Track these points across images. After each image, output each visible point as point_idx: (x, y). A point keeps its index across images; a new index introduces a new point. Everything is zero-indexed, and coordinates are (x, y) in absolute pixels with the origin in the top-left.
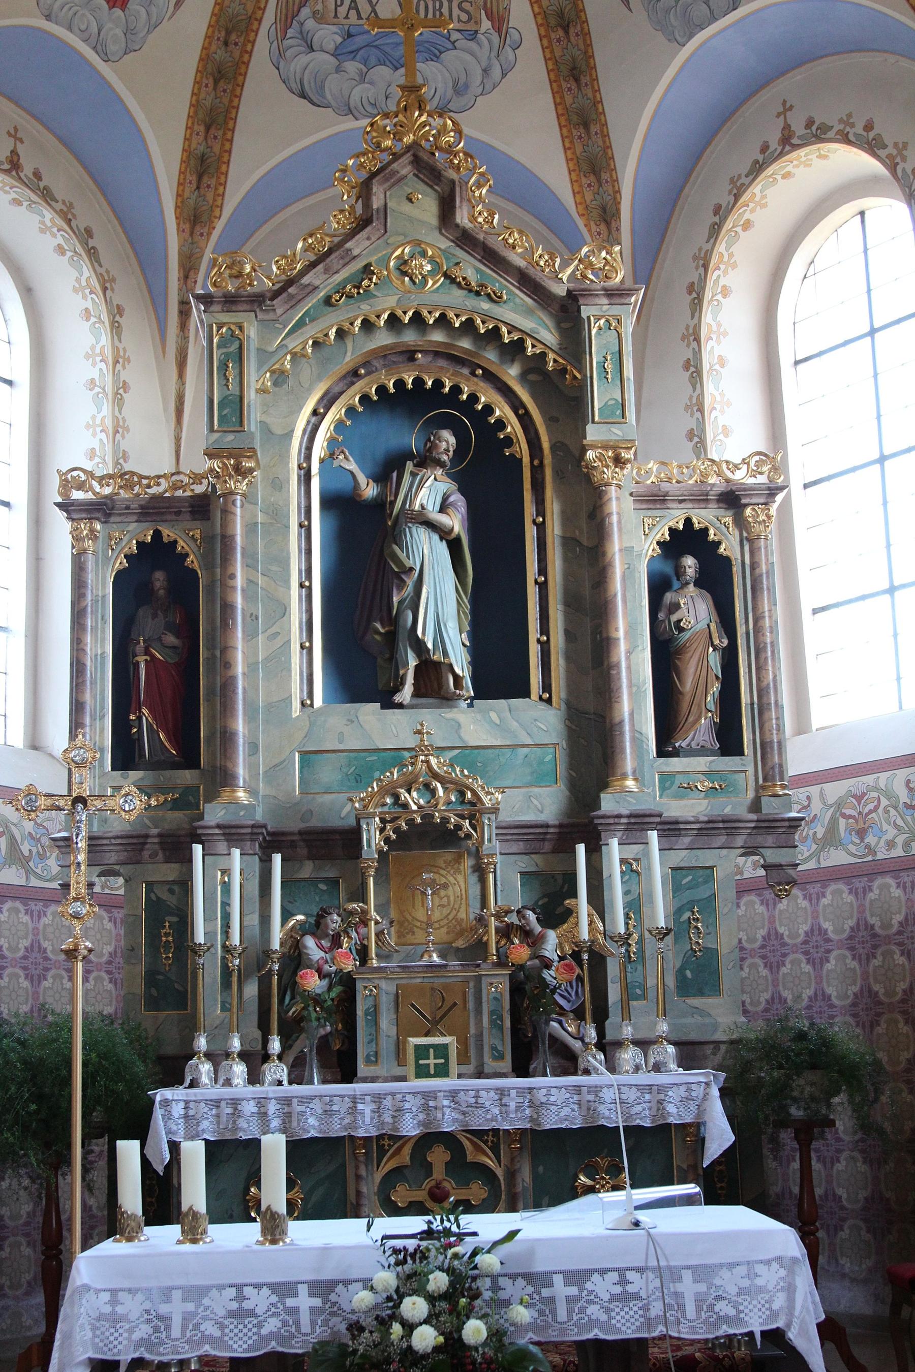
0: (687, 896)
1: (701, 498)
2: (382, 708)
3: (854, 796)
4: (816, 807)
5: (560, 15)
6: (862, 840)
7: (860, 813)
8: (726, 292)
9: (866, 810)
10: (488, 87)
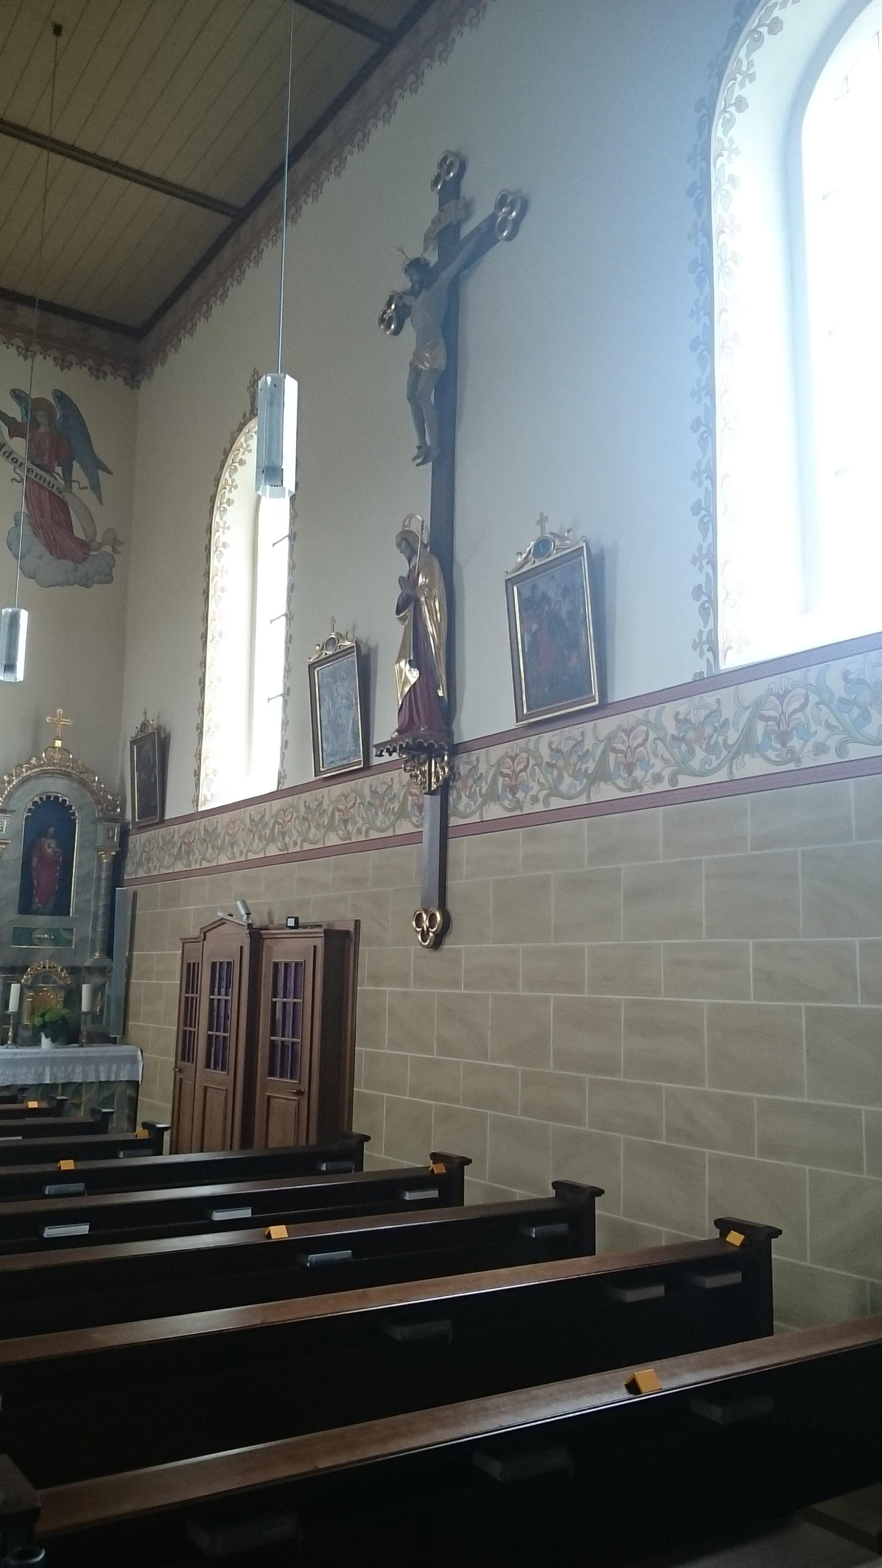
2: (401, 579)
3: (624, 731)
4: (728, 712)
6: (630, 774)
7: (514, 771)
8: (230, 502)
9: (791, 709)
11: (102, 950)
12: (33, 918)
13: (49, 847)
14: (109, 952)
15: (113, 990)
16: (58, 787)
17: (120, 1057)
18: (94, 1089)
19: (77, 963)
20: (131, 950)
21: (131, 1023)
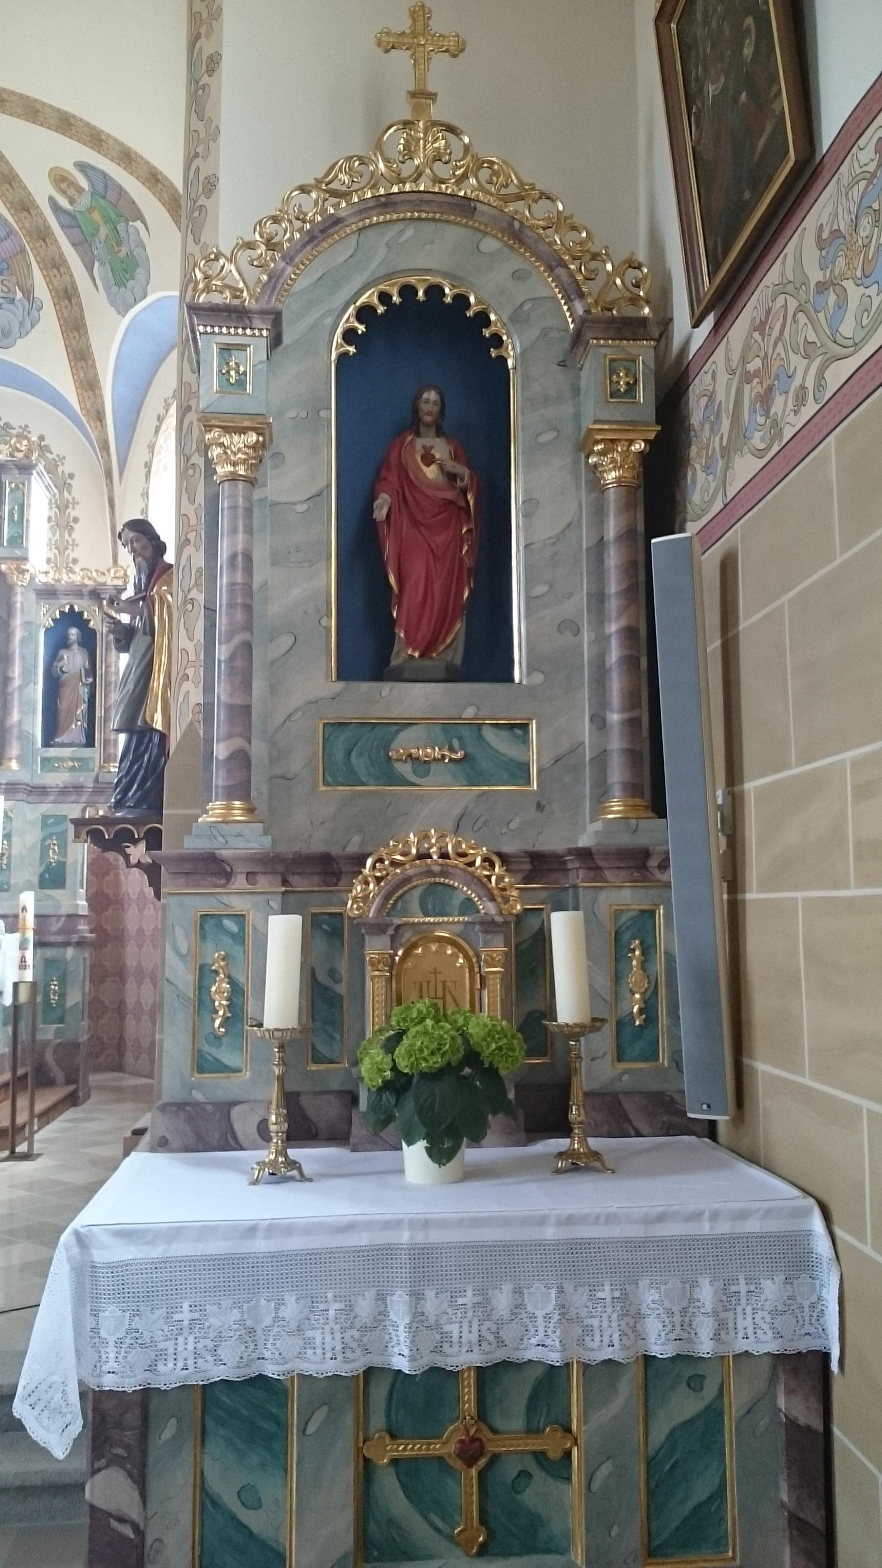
0: (50, 830)
1: (77, 592)
5: (66, 291)
10: (24, 333)
11: (632, 789)
12: (386, 688)
13: (429, 459)
14: (652, 792)
15: (684, 929)
16: (429, 257)
17: (718, 1242)
18: (627, 1389)
19: (553, 842)
20: (734, 775)
21: (763, 1068)
